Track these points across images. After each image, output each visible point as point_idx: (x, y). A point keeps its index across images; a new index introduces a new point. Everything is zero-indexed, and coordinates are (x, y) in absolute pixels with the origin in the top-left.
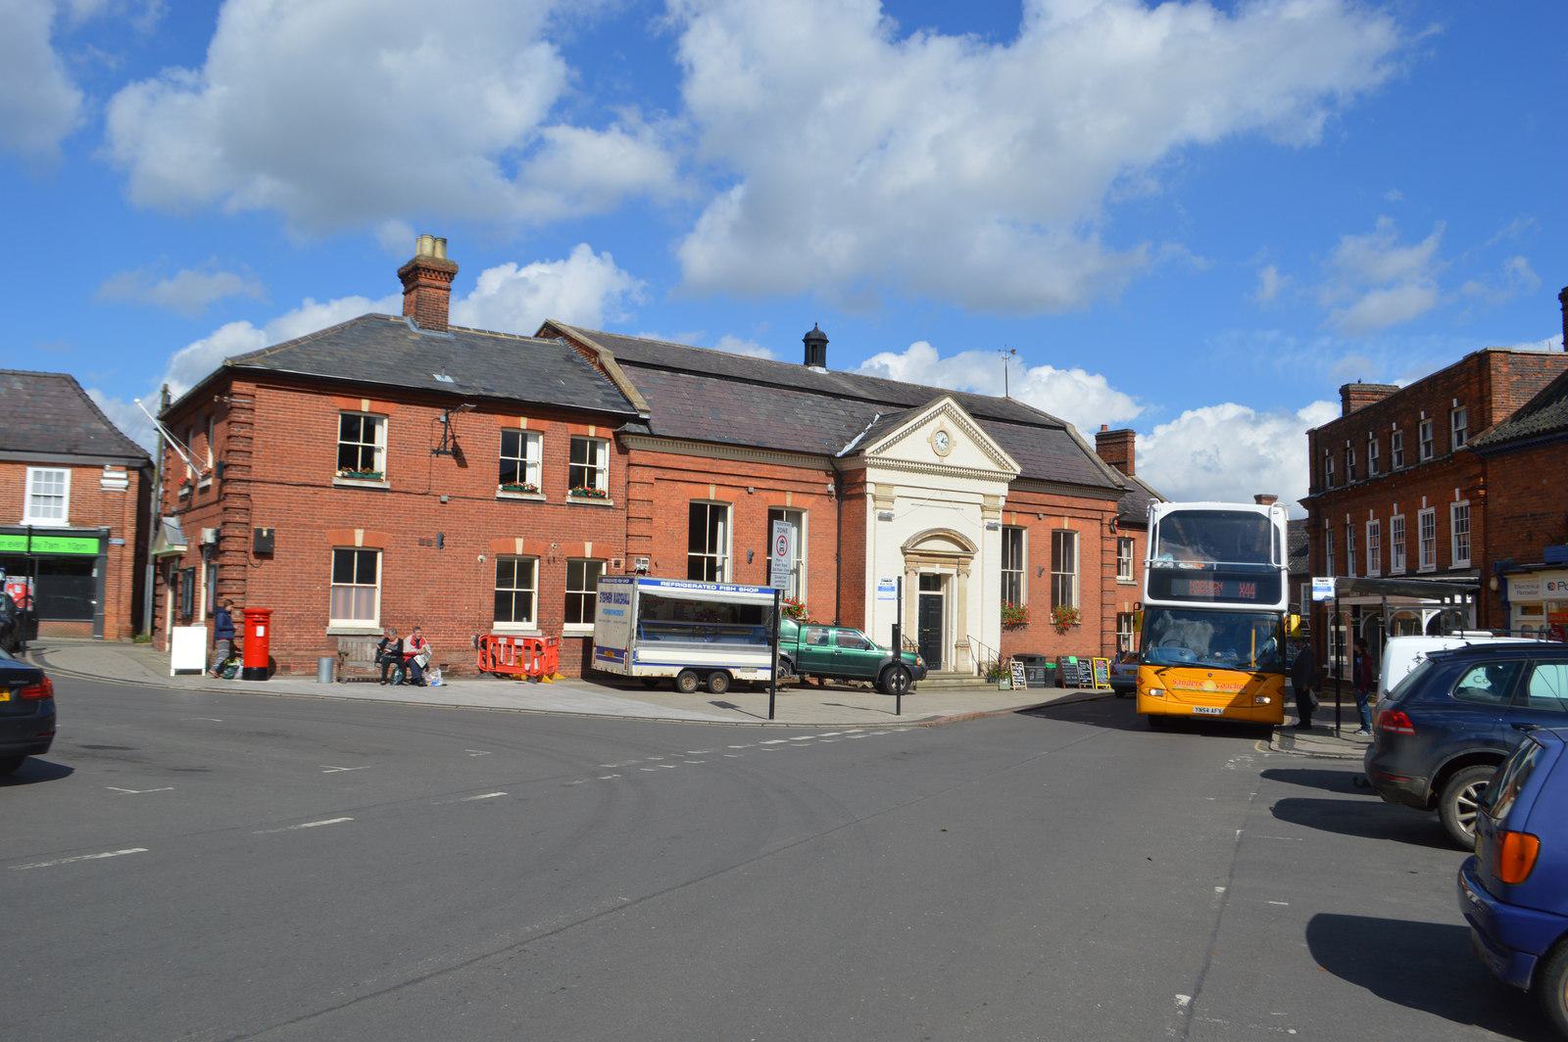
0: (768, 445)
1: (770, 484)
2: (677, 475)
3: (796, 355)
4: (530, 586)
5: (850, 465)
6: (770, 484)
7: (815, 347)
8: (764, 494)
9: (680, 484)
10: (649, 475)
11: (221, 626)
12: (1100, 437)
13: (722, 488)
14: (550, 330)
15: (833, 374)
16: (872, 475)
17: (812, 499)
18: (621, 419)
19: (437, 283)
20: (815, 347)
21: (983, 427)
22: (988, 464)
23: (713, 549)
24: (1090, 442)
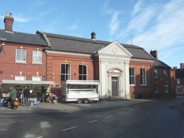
0: (78, 52)
1: (79, 59)
2: (58, 58)
3: (90, 37)
4: (86, 74)
5: (96, 55)
6: (79, 59)
7: (93, 35)
8: (78, 62)
9: (59, 60)
10: (51, 58)
11: (109, 72)
12: (151, 52)
13: (68, 61)
14: (38, 32)
15: (96, 40)
16: (100, 57)
17: (89, 63)
18: (45, 46)
19: (10, 22)
20: (93, 35)
21: (126, 49)
22: (126, 55)
23: (67, 73)
24: (149, 53)
